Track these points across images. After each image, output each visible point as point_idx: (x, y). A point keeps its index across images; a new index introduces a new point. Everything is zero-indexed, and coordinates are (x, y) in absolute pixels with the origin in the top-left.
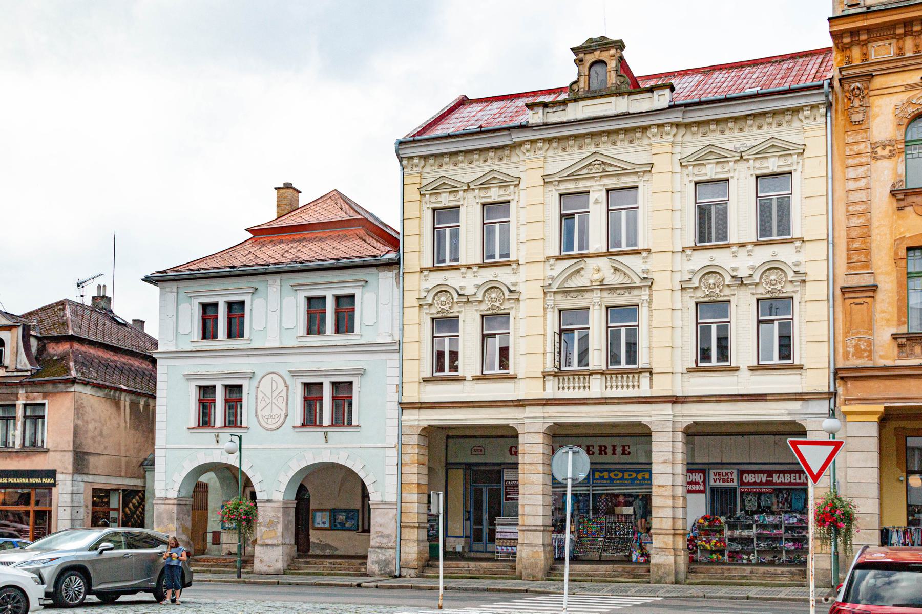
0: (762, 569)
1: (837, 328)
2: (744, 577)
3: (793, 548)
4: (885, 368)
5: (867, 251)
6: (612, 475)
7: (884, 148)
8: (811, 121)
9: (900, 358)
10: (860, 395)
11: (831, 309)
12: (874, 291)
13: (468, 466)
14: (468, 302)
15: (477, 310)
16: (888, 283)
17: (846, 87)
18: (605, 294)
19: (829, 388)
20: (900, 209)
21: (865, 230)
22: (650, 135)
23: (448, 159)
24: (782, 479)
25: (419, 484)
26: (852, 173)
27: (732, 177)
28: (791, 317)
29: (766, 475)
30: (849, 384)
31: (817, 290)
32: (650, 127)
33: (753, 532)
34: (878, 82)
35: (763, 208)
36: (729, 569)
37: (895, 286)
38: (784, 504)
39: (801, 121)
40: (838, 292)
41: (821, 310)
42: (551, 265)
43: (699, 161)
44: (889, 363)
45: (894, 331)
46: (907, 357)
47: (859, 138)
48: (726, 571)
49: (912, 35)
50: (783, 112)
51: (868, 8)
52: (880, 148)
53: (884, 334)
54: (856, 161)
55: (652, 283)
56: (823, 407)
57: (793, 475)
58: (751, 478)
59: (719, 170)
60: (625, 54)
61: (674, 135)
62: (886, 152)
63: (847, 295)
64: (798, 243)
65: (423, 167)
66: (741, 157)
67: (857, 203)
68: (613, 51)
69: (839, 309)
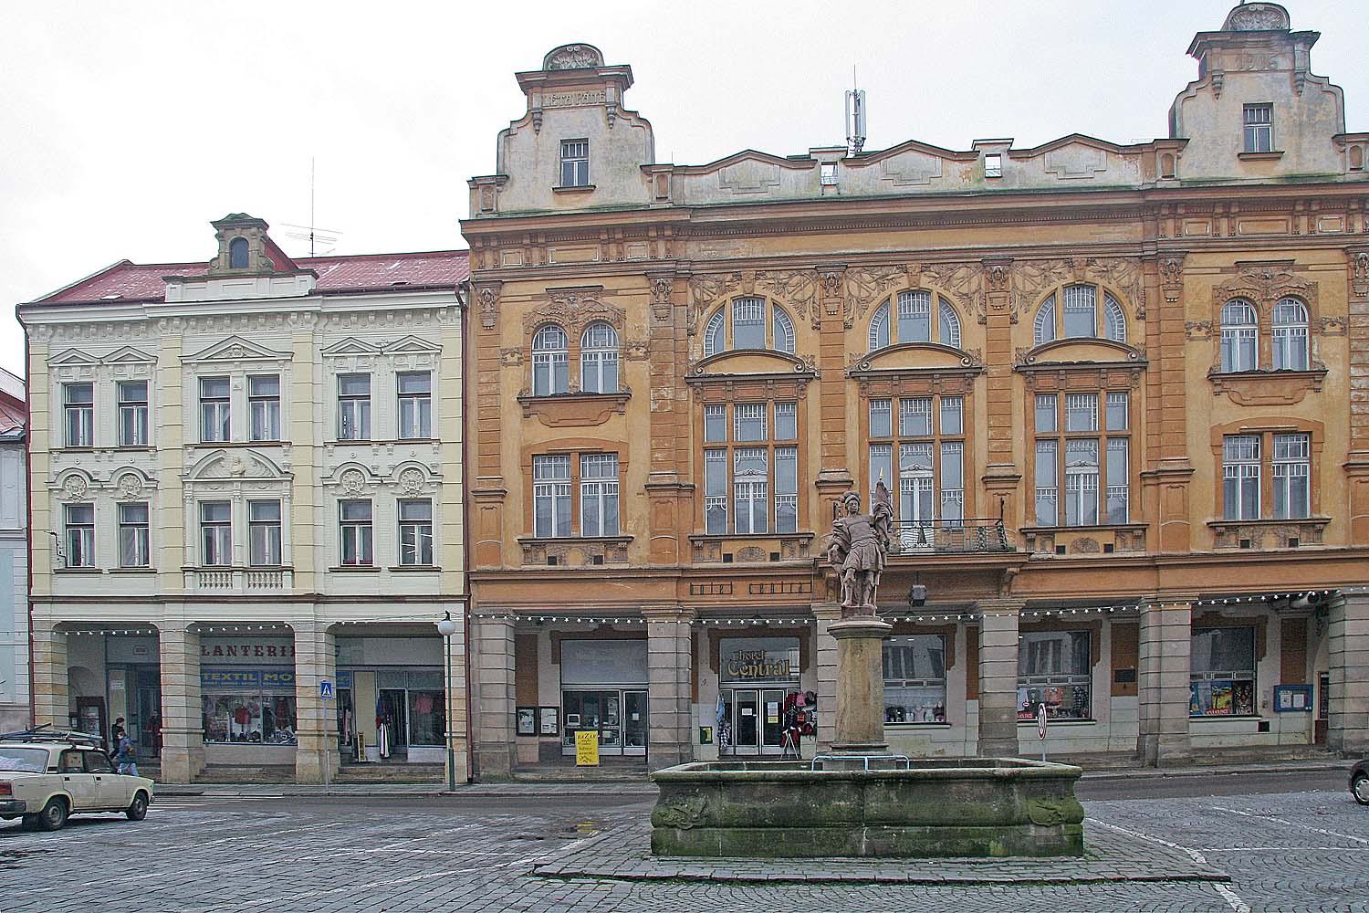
4: (1198, 556)
6: (281, 677)
13: (131, 667)
14: (102, 489)
18: (246, 487)
20: (526, 416)
23: (263, 320)
25: (54, 685)
34: (509, 289)
42: (189, 453)
43: (341, 352)
52: (509, 355)
55: (293, 478)
60: (271, 233)
61: (315, 324)
63: (989, 486)
64: (152, 452)
65: (51, 336)
68: (254, 230)
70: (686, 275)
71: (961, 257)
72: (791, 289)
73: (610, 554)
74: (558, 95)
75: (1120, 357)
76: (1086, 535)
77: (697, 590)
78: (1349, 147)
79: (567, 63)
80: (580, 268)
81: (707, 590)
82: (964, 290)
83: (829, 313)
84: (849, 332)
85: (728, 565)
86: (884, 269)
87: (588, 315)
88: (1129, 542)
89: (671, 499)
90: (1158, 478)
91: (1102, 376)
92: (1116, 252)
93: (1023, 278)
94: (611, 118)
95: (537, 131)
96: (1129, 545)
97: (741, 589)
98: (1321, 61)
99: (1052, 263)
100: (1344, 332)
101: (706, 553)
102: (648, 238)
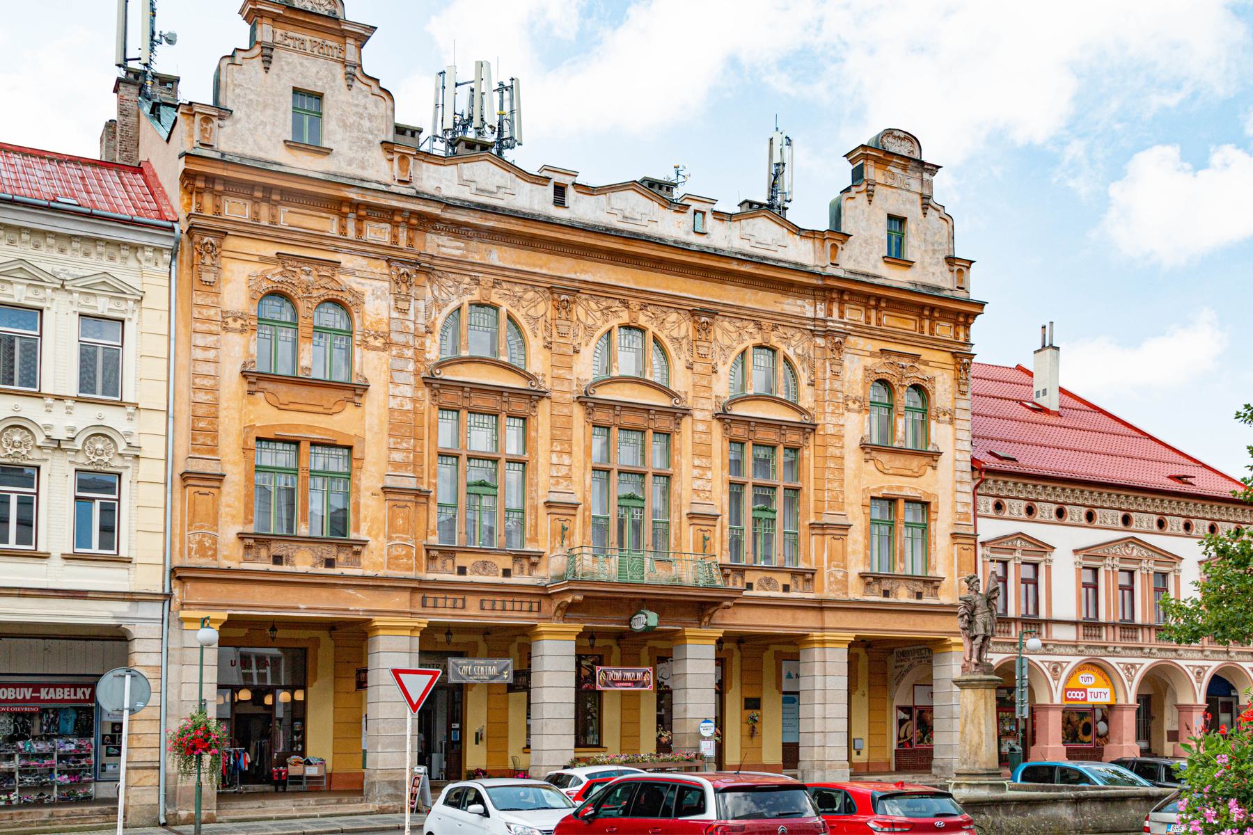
0: (65, 810)
1: (174, 517)
2: (44, 822)
3: (68, 781)
4: (229, 570)
5: (213, 433)
7: (235, 320)
8: (151, 265)
9: (245, 560)
10: (200, 600)
11: (169, 495)
12: (221, 481)
15: (71, 462)
16: (235, 474)
17: (197, 238)
19: (163, 588)
20: (251, 393)
21: (213, 410)
22: (142, 259)
24: (52, 695)
26: (199, 340)
27: (48, 308)
28: (116, 497)
29: (31, 690)
30: (189, 585)
31: (152, 470)
32: (143, 247)
33: (16, 764)
34: (231, 243)
35: (87, 357)
36: (21, 814)
37: (243, 478)
38: (49, 727)
39: (139, 261)
40: (177, 477)
41: (156, 495)
44: (234, 565)
45: (240, 529)
46: (252, 561)
47: (209, 301)
48: (15, 817)
49: (268, 202)
50: (119, 245)
51: (223, 155)
53: (229, 532)
54: (205, 327)
56: (155, 610)
57: (66, 690)
58: (66, 693)
59: (30, 294)
62: (238, 325)
64: (131, 409)
66: (63, 286)
67: (206, 376)
69: (177, 496)
70: (426, 268)
71: (673, 303)
72: (525, 304)
73: (342, 557)
74: (290, 34)
75: (663, 401)
76: (768, 575)
77: (430, 602)
78: (956, 268)
79: (894, 146)
80: (318, 239)
81: (441, 602)
82: (675, 334)
83: (562, 335)
84: (576, 356)
85: (886, 600)
86: (610, 301)
87: (322, 291)
88: (800, 583)
89: (409, 504)
90: (823, 528)
91: (504, 399)
92: (795, 322)
93: (724, 332)
94: (350, 77)
95: (267, 69)
96: (801, 587)
97: (473, 604)
98: (373, 58)
99: (745, 323)
100: (951, 422)
101: (439, 564)
102: (390, 222)
